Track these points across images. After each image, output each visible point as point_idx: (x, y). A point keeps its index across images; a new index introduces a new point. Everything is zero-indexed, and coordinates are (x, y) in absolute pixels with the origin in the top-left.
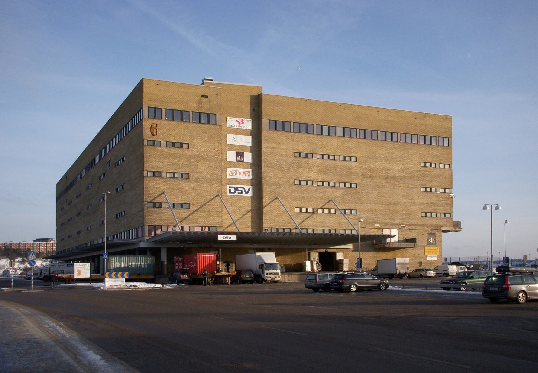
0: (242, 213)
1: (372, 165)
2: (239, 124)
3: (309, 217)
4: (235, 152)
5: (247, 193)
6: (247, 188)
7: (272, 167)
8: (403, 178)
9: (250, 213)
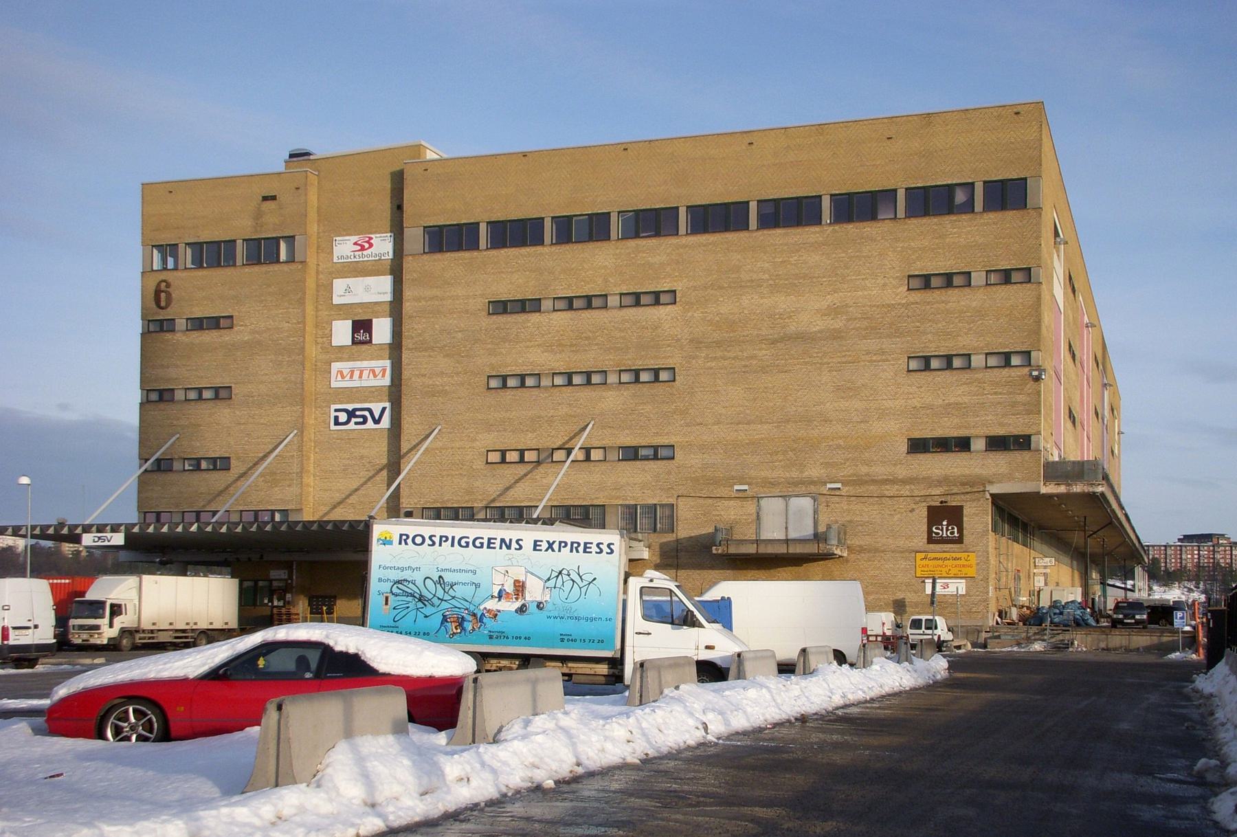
0: (365, 474)
1: (726, 307)
2: (363, 248)
3: (526, 475)
4: (350, 322)
5: (377, 422)
6: (376, 408)
7: (426, 350)
8: (836, 335)
9: (385, 473)
